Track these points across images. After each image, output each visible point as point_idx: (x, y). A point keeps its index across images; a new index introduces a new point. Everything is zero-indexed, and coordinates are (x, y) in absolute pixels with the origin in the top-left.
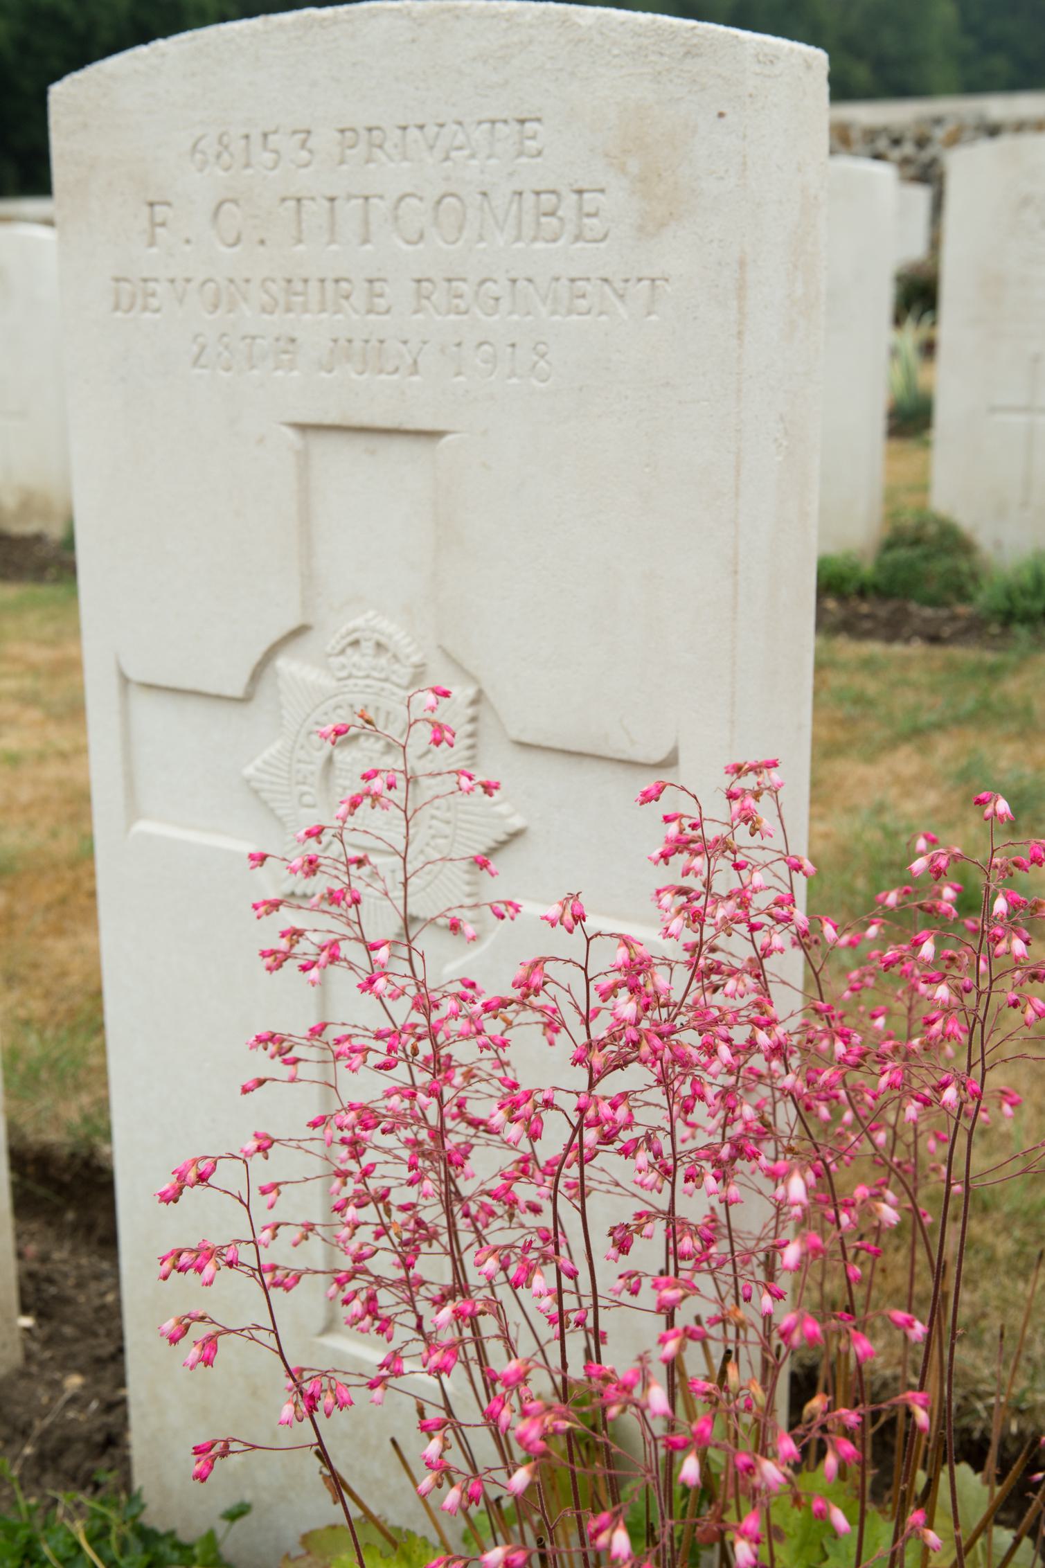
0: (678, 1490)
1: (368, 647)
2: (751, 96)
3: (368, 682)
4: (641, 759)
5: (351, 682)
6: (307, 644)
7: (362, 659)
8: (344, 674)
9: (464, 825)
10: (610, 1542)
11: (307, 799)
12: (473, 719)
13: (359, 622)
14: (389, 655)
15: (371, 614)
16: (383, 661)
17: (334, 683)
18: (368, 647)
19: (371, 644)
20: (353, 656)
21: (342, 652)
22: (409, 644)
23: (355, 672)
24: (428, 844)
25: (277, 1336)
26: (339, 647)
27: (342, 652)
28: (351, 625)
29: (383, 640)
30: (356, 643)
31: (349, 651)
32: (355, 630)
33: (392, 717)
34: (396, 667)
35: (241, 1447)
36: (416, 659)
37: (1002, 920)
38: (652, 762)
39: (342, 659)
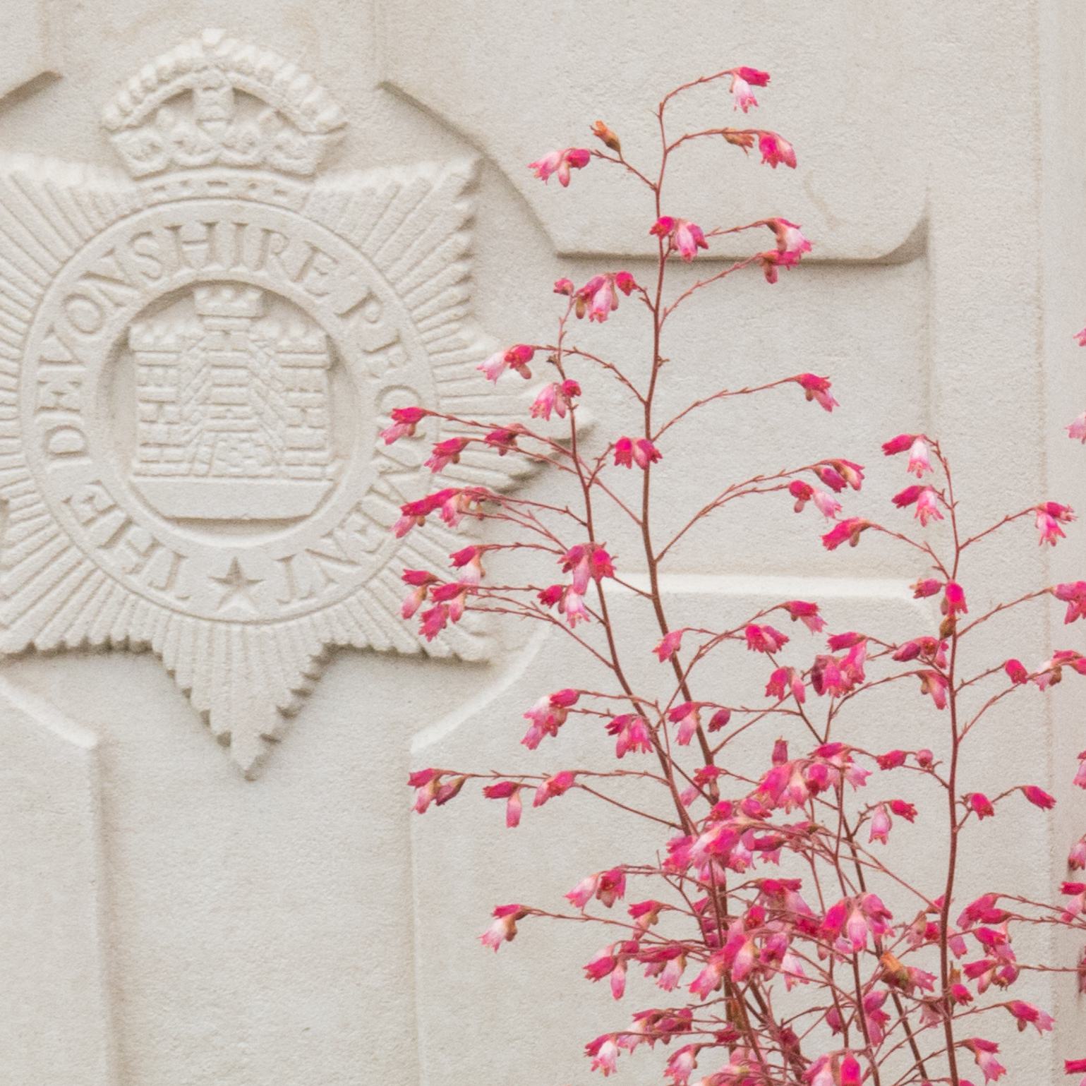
0: (940, 939)
1: (213, 103)
2: (904, 499)
3: (216, 174)
4: (853, 254)
5: (172, 179)
6: (49, 113)
7: (207, 130)
8: (157, 163)
11: (65, 440)
12: (469, 223)
13: (188, 52)
14: (267, 113)
15: (212, 36)
16: (250, 126)
17: (131, 188)
18: (213, 103)
19: (223, 95)
20: (178, 125)
21: (150, 118)
22: (310, 89)
23: (183, 157)
24: (372, 490)
25: (590, 530)
26: (139, 111)
27: (150, 118)
28: (166, 61)
29: (251, 84)
30: (184, 97)
31: (165, 115)
32: (179, 72)
34: (285, 135)
36: (329, 115)
38: (876, 256)
39: (148, 133)
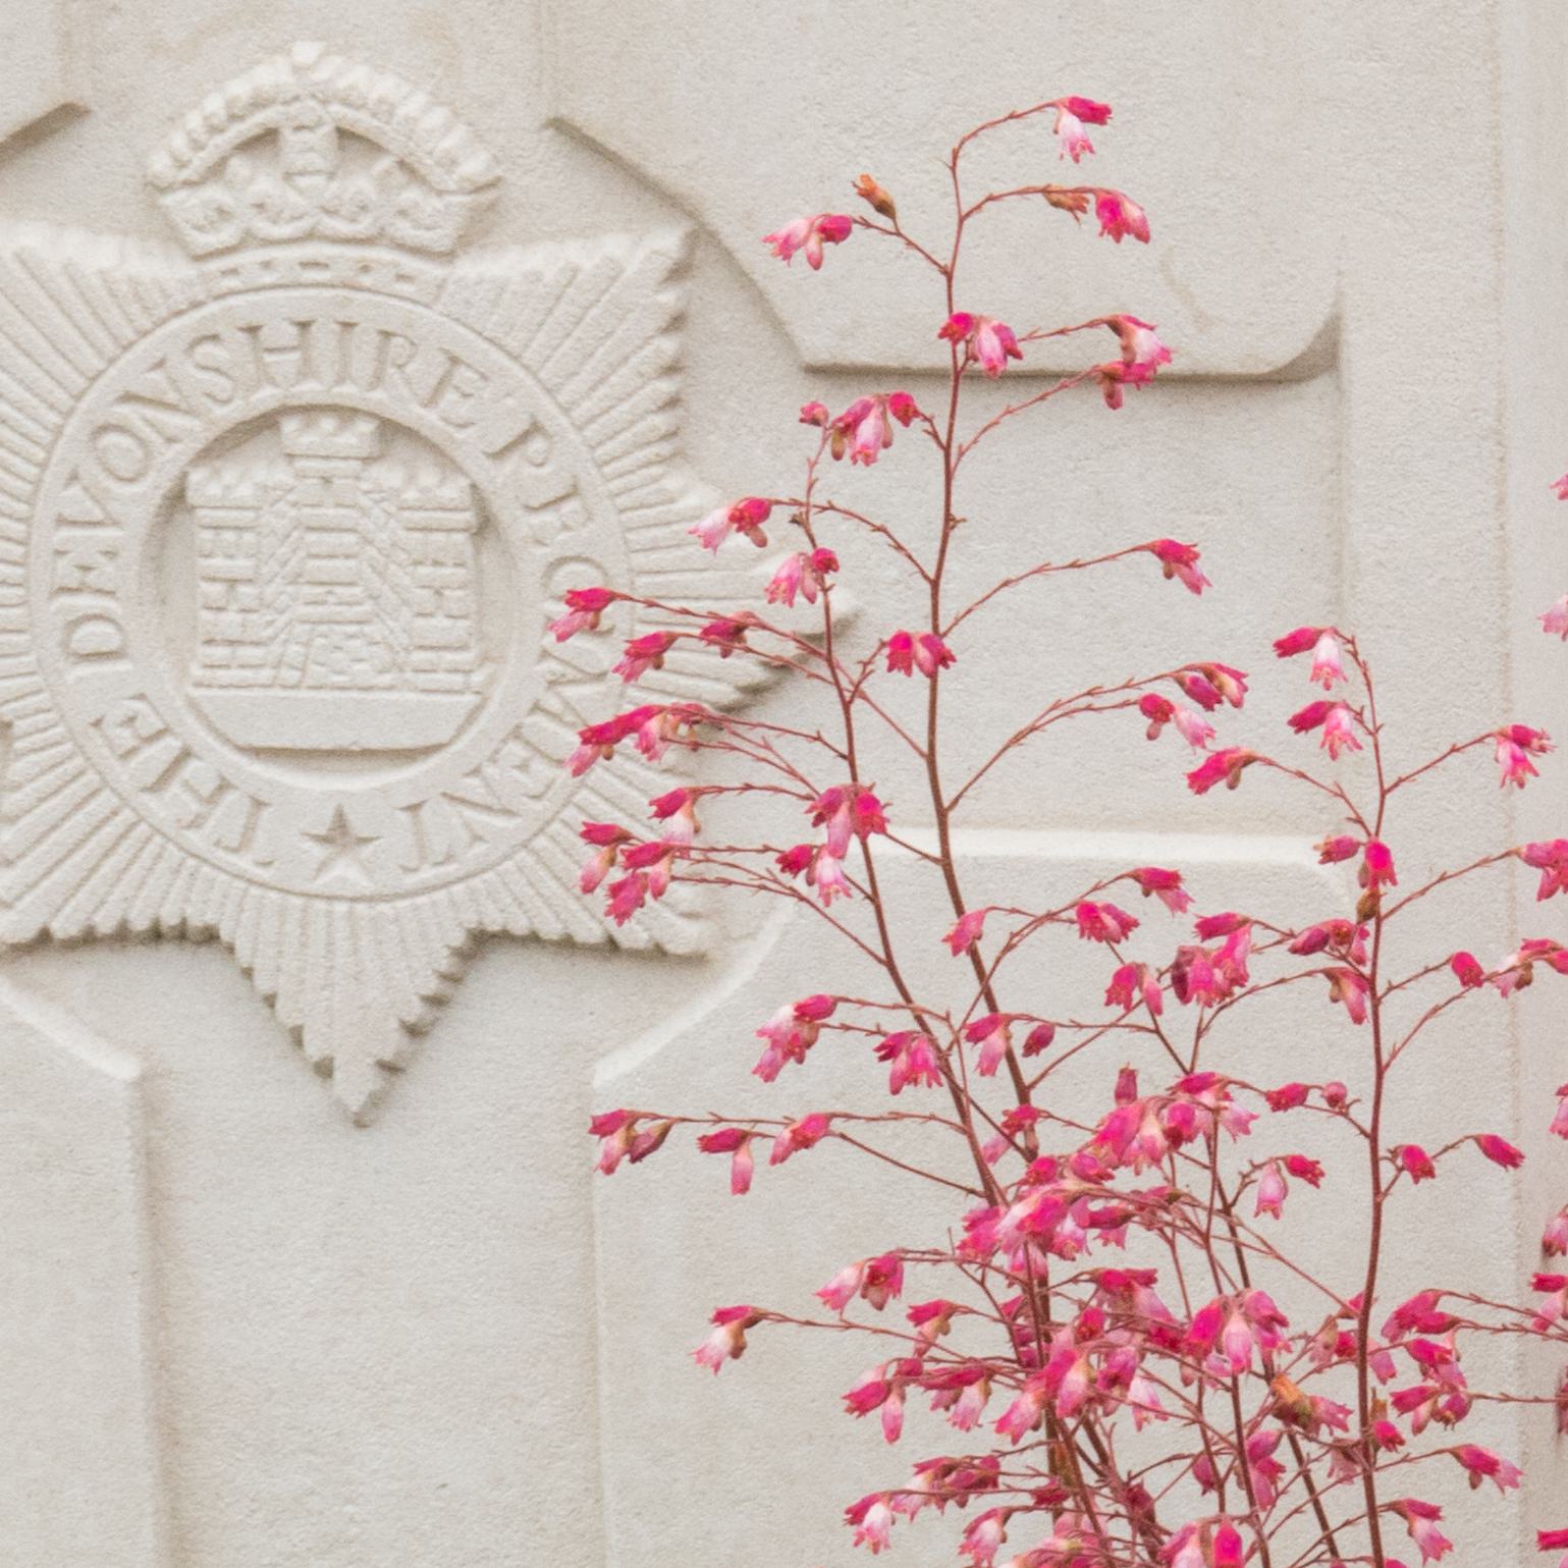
1: (307, 149)
3: (311, 251)
4: (1231, 367)
5: (249, 258)
7: (298, 188)
8: (226, 235)
9: (102, 337)
10: (1161, 1168)
11: (93, 635)
12: (677, 322)
13: (271, 75)
14: (385, 163)
15: (306, 52)
16: (361, 183)
17: (189, 271)
18: (307, 149)
19: (322, 137)
20: (258, 180)
21: (216, 170)
22: (447, 129)
23: (264, 227)
26: (200, 161)
27: (216, 170)
28: (240, 89)
29: (363, 122)
30: (266, 140)
31: (239, 166)
32: (258, 104)
33: (537, 445)
34: (412, 195)
35: (1064, 915)
36: (474, 166)
37: (837, 892)
38: (1264, 369)
39: (214, 193)
